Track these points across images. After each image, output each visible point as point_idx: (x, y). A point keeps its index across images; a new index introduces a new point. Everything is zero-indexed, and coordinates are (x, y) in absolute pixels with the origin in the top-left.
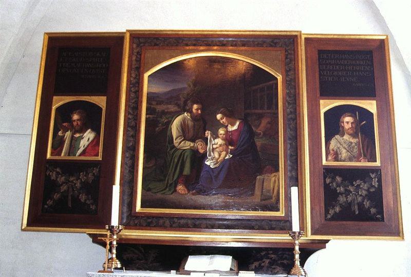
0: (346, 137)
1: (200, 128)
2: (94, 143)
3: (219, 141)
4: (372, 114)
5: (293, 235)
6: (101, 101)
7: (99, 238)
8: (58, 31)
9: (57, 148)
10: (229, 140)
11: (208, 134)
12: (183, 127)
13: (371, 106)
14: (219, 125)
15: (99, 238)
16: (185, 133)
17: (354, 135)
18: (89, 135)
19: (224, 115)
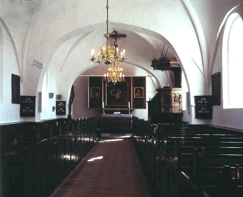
0: (138, 93)
1: (115, 92)
2: (98, 95)
3: (118, 94)
4: (142, 90)
5: (129, 109)
6: (99, 88)
7: (129, 102)
8: (194, 111)
9: (136, 96)
10: (120, 94)
11: (116, 93)
12: (113, 92)
13: (143, 88)
14: (118, 92)
15: (129, 102)
16: (113, 93)
17: (139, 93)
18: (97, 94)
19: (119, 90)
